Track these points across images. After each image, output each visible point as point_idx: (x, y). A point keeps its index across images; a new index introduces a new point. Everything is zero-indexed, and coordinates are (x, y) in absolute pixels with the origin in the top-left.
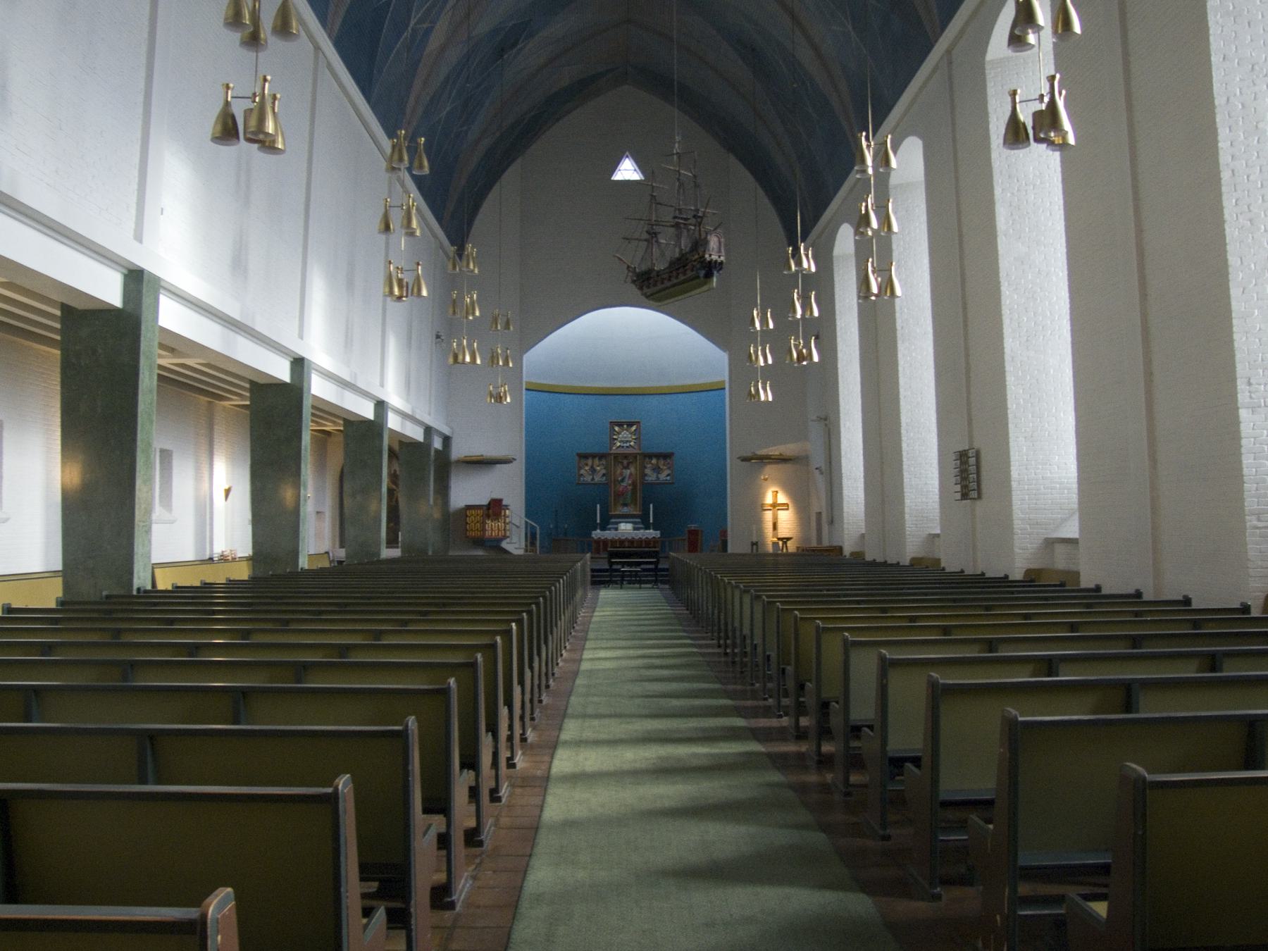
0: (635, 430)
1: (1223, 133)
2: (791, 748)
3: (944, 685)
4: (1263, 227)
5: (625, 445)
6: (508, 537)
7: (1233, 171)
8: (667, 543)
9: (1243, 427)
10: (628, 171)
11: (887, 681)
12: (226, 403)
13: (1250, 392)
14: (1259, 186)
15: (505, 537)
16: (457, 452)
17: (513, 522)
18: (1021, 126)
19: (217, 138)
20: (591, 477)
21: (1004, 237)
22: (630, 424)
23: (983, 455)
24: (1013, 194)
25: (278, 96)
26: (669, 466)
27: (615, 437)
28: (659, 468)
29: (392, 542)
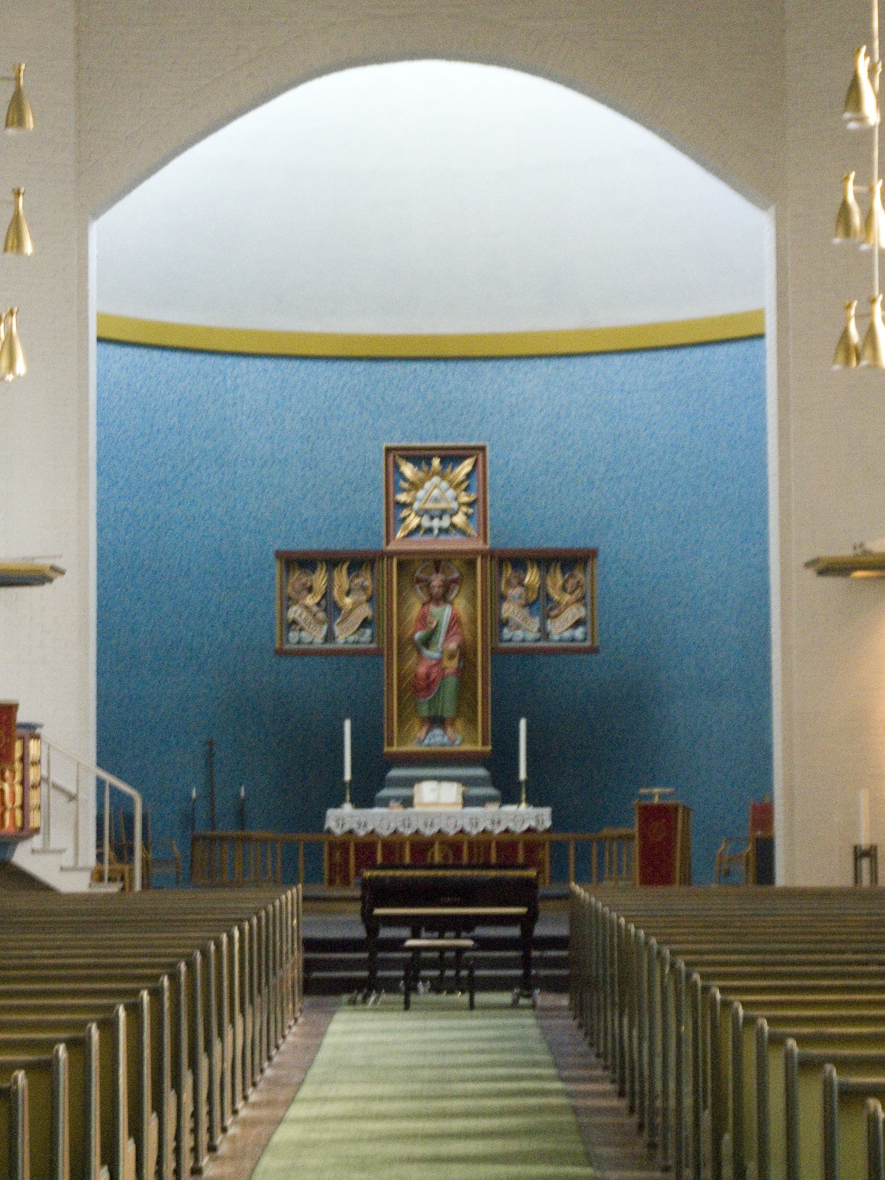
0: (469, 475)
5: (436, 523)
27: (402, 498)
28: (548, 598)
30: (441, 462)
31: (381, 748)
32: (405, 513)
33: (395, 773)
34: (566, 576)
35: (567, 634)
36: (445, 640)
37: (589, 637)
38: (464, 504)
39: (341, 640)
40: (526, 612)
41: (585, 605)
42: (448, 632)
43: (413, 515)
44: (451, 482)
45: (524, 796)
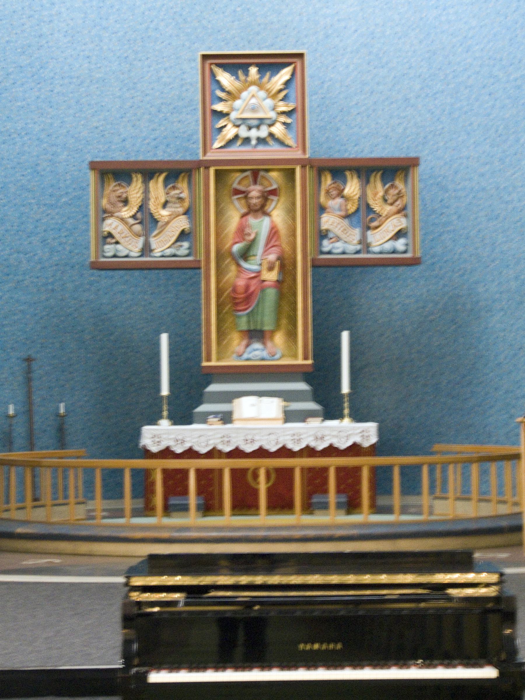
0: (287, 83)
5: (254, 133)
8: (425, 470)
20: (141, 241)
26: (399, 203)
27: (219, 107)
28: (369, 209)
30: (259, 71)
31: (200, 361)
32: (222, 123)
33: (213, 388)
34: (387, 186)
35: (388, 246)
36: (265, 251)
37: (410, 248)
38: (283, 113)
39: (157, 253)
40: (346, 223)
41: (406, 216)
42: (267, 244)
43: (230, 126)
44: (268, 91)
45: (346, 411)
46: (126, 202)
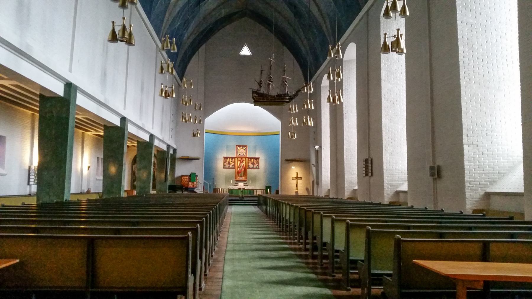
1: (461, 49)
2: (303, 253)
3: (351, 224)
4: (473, 82)
6: (197, 187)
7: (464, 62)
9: (465, 151)
10: (246, 51)
11: (320, 147)
12: (89, 133)
13: (467, 139)
14: (473, 67)
15: (196, 187)
16: (179, 155)
17: (199, 182)
18: (387, 46)
19: (110, 40)
21: (384, 82)
22: (244, 146)
23: (374, 161)
24: (388, 66)
25: (132, 25)
29: (154, 188)
46: (227, 161)
